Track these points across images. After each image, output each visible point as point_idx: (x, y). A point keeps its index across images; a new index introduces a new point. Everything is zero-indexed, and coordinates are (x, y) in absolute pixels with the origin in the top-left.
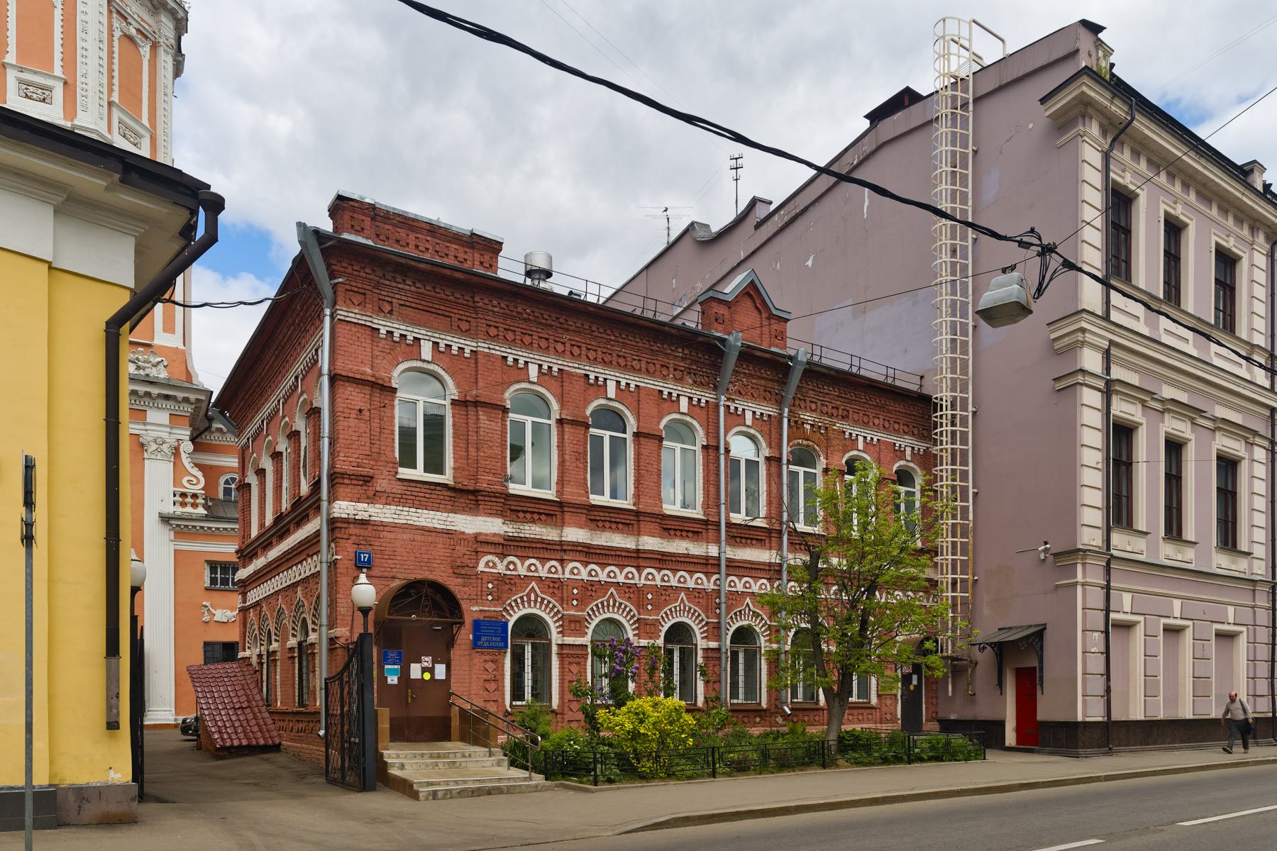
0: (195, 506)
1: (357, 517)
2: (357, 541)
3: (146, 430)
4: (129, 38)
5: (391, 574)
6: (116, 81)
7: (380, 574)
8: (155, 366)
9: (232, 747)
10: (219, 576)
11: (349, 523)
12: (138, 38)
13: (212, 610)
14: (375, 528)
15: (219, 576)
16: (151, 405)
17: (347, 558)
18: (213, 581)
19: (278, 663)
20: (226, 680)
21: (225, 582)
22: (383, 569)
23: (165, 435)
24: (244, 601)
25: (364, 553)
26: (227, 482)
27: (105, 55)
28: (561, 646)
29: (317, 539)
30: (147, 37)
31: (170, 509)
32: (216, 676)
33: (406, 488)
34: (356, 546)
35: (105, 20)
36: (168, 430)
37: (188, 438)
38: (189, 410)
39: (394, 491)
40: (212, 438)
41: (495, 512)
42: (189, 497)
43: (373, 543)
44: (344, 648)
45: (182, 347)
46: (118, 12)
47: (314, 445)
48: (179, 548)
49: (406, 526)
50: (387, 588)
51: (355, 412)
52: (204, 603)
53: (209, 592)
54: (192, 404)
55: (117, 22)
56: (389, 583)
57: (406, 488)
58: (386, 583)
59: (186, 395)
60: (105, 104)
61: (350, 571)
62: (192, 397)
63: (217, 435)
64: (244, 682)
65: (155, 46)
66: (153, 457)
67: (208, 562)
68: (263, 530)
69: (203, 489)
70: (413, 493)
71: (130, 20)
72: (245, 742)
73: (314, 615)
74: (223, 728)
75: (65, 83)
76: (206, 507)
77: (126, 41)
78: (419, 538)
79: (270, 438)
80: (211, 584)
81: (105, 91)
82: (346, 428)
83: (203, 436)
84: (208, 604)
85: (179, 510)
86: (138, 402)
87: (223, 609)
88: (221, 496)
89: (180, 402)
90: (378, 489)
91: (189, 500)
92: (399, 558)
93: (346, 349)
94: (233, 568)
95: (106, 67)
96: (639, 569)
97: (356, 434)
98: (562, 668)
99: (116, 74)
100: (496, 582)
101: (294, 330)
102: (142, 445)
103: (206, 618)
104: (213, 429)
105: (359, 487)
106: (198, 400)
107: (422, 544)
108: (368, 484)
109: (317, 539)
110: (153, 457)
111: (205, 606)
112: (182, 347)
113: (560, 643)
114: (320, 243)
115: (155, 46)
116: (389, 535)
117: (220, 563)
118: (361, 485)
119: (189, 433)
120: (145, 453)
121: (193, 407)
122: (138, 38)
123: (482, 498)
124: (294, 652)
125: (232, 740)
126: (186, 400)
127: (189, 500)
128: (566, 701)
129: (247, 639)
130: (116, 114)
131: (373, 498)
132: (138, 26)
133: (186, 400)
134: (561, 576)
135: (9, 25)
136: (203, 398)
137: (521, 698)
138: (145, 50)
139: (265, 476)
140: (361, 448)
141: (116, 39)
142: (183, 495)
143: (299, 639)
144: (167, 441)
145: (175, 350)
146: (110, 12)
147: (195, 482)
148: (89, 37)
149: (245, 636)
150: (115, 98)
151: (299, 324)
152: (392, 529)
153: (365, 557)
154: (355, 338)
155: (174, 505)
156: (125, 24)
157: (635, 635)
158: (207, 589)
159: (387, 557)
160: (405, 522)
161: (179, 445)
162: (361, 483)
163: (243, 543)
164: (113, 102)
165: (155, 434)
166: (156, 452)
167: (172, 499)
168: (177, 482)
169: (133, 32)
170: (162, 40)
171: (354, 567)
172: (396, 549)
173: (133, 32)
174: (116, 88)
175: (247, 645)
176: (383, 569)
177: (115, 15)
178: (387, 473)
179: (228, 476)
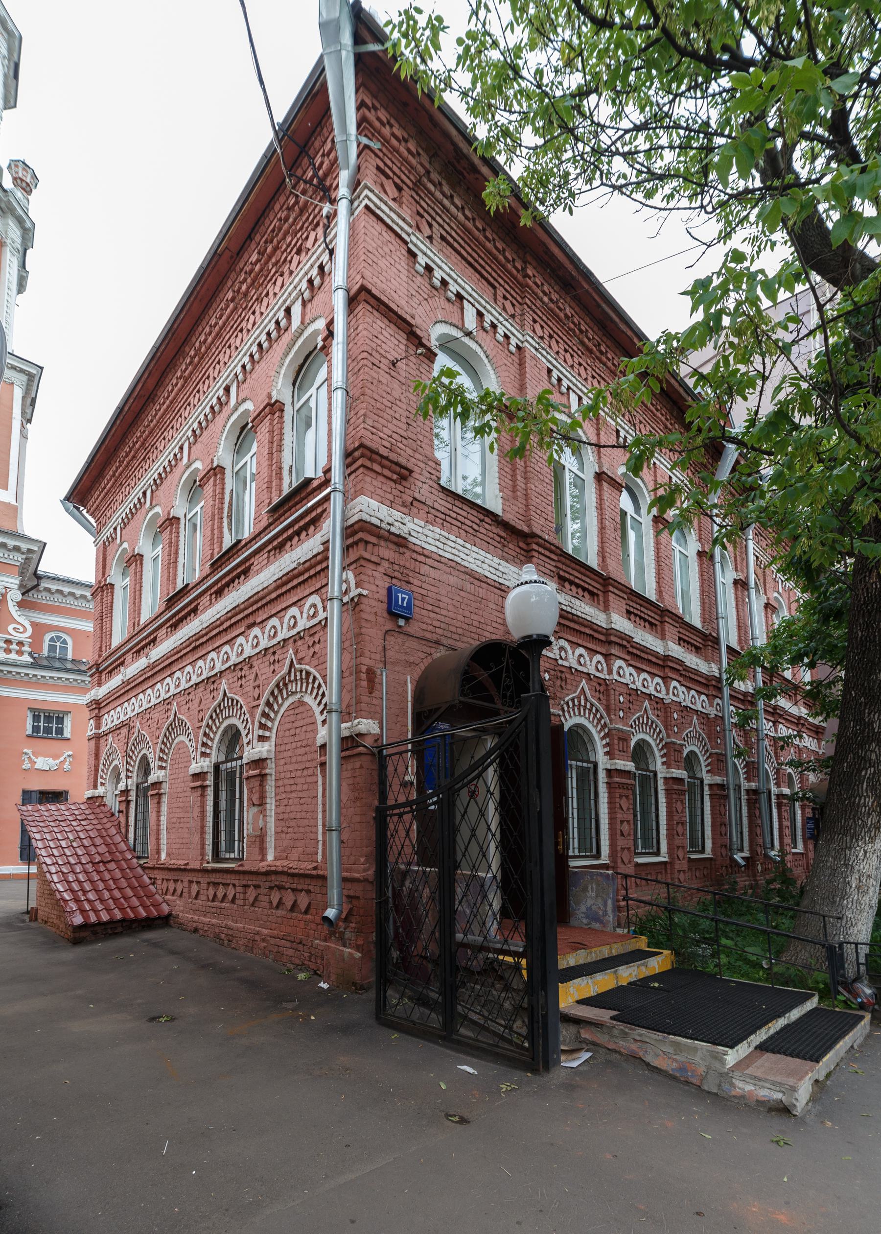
0: (20, 653)
1: (393, 529)
2: (390, 572)
5: (435, 637)
7: (420, 634)
9: (100, 924)
10: (41, 724)
11: (379, 537)
14: (415, 556)
15: (41, 724)
17: (376, 596)
18: (36, 729)
19: (165, 799)
20: (74, 823)
21: (48, 730)
22: (424, 627)
24: (98, 727)
25: (402, 593)
26: (52, 639)
28: (609, 772)
29: (324, 565)
32: (60, 818)
33: (450, 506)
34: (388, 579)
39: (436, 505)
41: (548, 572)
43: (411, 580)
44: (373, 754)
47: (271, 458)
49: (454, 564)
50: (429, 660)
51: (386, 362)
54: (23, 553)
56: (433, 651)
57: (450, 506)
58: (428, 650)
59: (17, 544)
61: (380, 619)
62: (24, 546)
63: (45, 594)
64: (99, 827)
68: (137, 629)
69: (29, 637)
70: (459, 518)
72: (118, 915)
73: (205, 735)
74: (80, 893)
78: (468, 587)
79: (158, 509)
82: (375, 382)
83: (30, 594)
84: (29, 751)
87: (45, 756)
88: (45, 652)
89: (9, 550)
90: (417, 496)
91: (14, 647)
92: (444, 612)
93: (375, 260)
94: (58, 717)
96: (665, 679)
97: (389, 397)
98: (611, 798)
100: (552, 672)
101: (235, 308)
103: (26, 765)
104: (41, 588)
105: (393, 484)
106: (30, 551)
107: (471, 597)
108: (404, 483)
109: (324, 565)
112: (13, 502)
113: (609, 767)
114: (358, 40)
116: (433, 573)
117: (44, 711)
118: (395, 481)
119: (17, 582)
123: (535, 547)
124: (204, 780)
125: (96, 912)
126: (17, 549)
127: (14, 647)
128: (619, 848)
129: (100, 773)
131: (411, 505)
133: (17, 549)
134: (607, 677)
136: (36, 549)
137: (651, 845)
139: (141, 564)
140: (394, 421)
143: (214, 759)
145: (8, 505)
147: (21, 629)
149: (96, 770)
151: (246, 294)
152: (436, 564)
153: (403, 599)
154: (387, 250)
157: (663, 763)
158: (28, 736)
159: (430, 607)
160: (451, 557)
162: (395, 477)
163: (100, 656)
170: (8, 241)
171: (385, 615)
172: (442, 598)
175: (100, 780)
176: (424, 627)
178: (428, 475)
179: (54, 634)
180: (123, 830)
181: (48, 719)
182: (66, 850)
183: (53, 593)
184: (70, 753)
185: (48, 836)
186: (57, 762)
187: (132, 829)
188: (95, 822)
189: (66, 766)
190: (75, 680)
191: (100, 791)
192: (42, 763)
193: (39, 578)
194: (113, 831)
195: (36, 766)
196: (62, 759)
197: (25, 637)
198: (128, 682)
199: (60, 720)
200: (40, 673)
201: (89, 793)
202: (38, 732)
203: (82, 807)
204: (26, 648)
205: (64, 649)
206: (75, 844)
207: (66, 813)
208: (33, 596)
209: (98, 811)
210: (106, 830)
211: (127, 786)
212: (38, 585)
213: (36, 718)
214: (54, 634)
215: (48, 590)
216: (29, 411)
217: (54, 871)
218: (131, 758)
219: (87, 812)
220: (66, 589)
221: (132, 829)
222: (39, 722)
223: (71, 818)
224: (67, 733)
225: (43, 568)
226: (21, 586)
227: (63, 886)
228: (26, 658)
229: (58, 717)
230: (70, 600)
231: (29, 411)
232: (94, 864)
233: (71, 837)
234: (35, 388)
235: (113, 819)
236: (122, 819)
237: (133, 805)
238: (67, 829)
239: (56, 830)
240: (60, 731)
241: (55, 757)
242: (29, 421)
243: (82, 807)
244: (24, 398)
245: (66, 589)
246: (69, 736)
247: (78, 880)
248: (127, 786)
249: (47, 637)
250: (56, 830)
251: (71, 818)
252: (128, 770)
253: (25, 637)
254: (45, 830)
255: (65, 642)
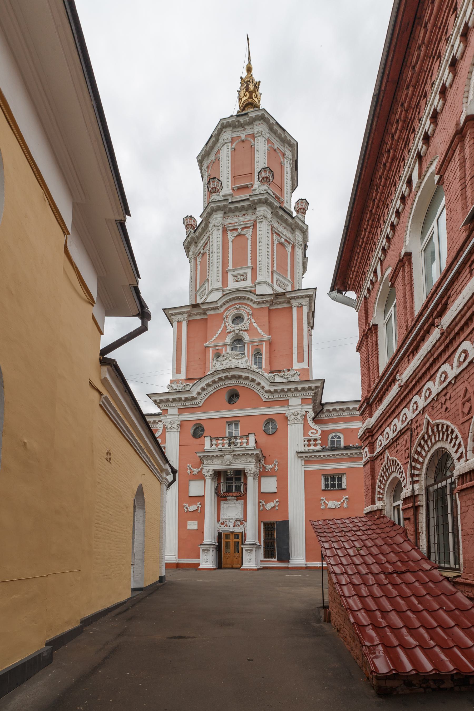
0: (315, 445)
3: (289, 410)
4: (281, 244)
6: (275, 262)
8: (293, 376)
10: (330, 483)
12: (286, 244)
13: (326, 502)
15: (330, 483)
16: (291, 396)
18: (327, 486)
20: (359, 533)
21: (333, 486)
23: (299, 410)
24: (372, 451)
26: (332, 438)
27: (270, 261)
30: (289, 243)
31: (302, 449)
32: (345, 529)
35: (270, 235)
36: (301, 407)
37: (311, 410)
38: (312, 394)
40: (324, 416)
42: (312, 441)
45: (307, 367)
46: (276, 233)
48: (306, 469)
52: (322, 498)
53: (324, 491)
55: (275, 237)
59: (310, 385)
60: (270, 271)
62: (313, 385)
63: (326, 414)
64: (383, 535)
65: (293, 247)
66: (293, 423)
67: (323, 475)
69: (320, 436)
71: (282, 235)
75: (270, 343)
76: (321, 445)
77: (280, 246)
80: (325, 488)
81: (270, 265)
84: (324, 499)
85: (307, 448)
86: (284, 396)
87: (333, 501)
91: (312, 442)
94: (338, 478)
95: (270, 252)
99: (275, 259)
102: (287, 418)
103: (323, 506)
106: (317, 387)
110: (293, 423)
111: (322, 500)
115: (293, 247)
117: (330, 475)
119: (311, 407)
120: (288, 422)
121: (314, 392)
122: (286, 244)
126: (310, 388)
127: (312, 442)
129: (377, 489)
130: (275, 276)
132: (285, 238)
133: (310, 388)
135: (229, 255)
136: (319, 385)
138: (289, 249)
141: (275, 244)
142: (309, 440)
144: (300, 413)
146: (272, 233)
147: (315, 432)
148: (262, 244)
150: (275, 269)
155: (304, 446)
156: (279, 238)
158: (323, 490)
161: (306, 414)
163: (369, 392)
164: (274, 270)
165: (293, 411)
166: (294, 420)
167: (303, 443)
168: (305, 434)
169: (283, 240)
173: (283, 240)
174: (275, 265)
175: (377, 496)
177: (274, 234)
179: (333, 435)
180: (412, 538)
181: (333, 479)
182: (354, 559)
183: (331, 412)
184: (347, 497)
185: (336, 545)
186: (340, 503)
187: (423, 537)
188: (378, 531)
189: (345, 505)
190: (347, 454)
191: (379, 505)
192: (331, 504)
193: (323, 405)
194: (400, 539)
195: (328, 507)
196: (342, 501)
197: (317, 436)
198: (407, 384)
199: (340, 479)
200: (326, 453)
201: (368, 509)
202: (328, 487)
203: (364, 520)
204: (319, 442)
205: (339, 442)
206: (362, 552)
207: (351, 525)
208: (321, 417)
209: (378, 522)
210: (391, 538)
211: (413, 491)
212: (323, 409)
213: (326, 480)
214: (333, 435)
215: (328, 411)
216: (311, 321)
217: (340, 554)
218: (416, 461)
219: (369, 523)
220: (338, 407)
221: (423, 537)
222: (328, 481)
223: (355, 529)
224: (344, 486)
225: (323, 401)
226: (314, 410)
227: (347, 560)
228: (319, 447)
229: (338, 478)
230: (341, 413)
231: (311, 321)
232: (387, 575)
233: (358, 545)
234: (313, 304)
235: (394, 528)
236: (410, 527)
237: (423, 511)
238: (353, 538)
239: (343, 539)
240: (340, 485)
241: (338, 500)
242: (312, 328)
243: (364, 520)
244: (308, 313)
245: (338, 407)
246: (345, 487)
247: (359, 573)
248: (413, 491)
249: (330, 437)
250: (343, 539)
251: (355, 529)
252: (412, 475)
253: (317, 436)
254: (333, 539)
255: (339, 437)
